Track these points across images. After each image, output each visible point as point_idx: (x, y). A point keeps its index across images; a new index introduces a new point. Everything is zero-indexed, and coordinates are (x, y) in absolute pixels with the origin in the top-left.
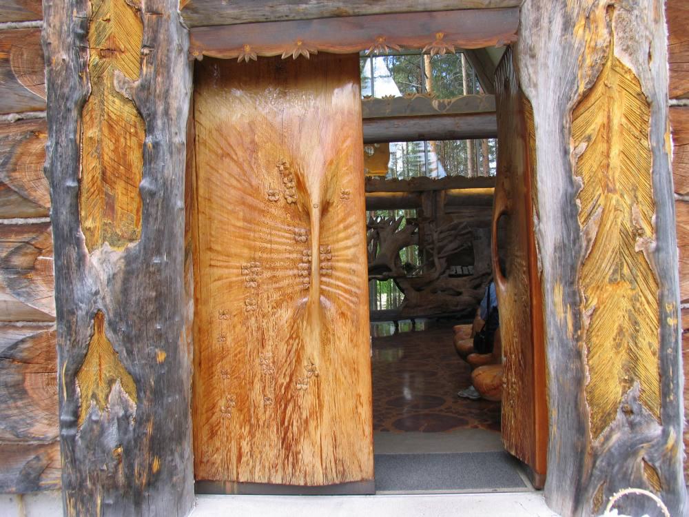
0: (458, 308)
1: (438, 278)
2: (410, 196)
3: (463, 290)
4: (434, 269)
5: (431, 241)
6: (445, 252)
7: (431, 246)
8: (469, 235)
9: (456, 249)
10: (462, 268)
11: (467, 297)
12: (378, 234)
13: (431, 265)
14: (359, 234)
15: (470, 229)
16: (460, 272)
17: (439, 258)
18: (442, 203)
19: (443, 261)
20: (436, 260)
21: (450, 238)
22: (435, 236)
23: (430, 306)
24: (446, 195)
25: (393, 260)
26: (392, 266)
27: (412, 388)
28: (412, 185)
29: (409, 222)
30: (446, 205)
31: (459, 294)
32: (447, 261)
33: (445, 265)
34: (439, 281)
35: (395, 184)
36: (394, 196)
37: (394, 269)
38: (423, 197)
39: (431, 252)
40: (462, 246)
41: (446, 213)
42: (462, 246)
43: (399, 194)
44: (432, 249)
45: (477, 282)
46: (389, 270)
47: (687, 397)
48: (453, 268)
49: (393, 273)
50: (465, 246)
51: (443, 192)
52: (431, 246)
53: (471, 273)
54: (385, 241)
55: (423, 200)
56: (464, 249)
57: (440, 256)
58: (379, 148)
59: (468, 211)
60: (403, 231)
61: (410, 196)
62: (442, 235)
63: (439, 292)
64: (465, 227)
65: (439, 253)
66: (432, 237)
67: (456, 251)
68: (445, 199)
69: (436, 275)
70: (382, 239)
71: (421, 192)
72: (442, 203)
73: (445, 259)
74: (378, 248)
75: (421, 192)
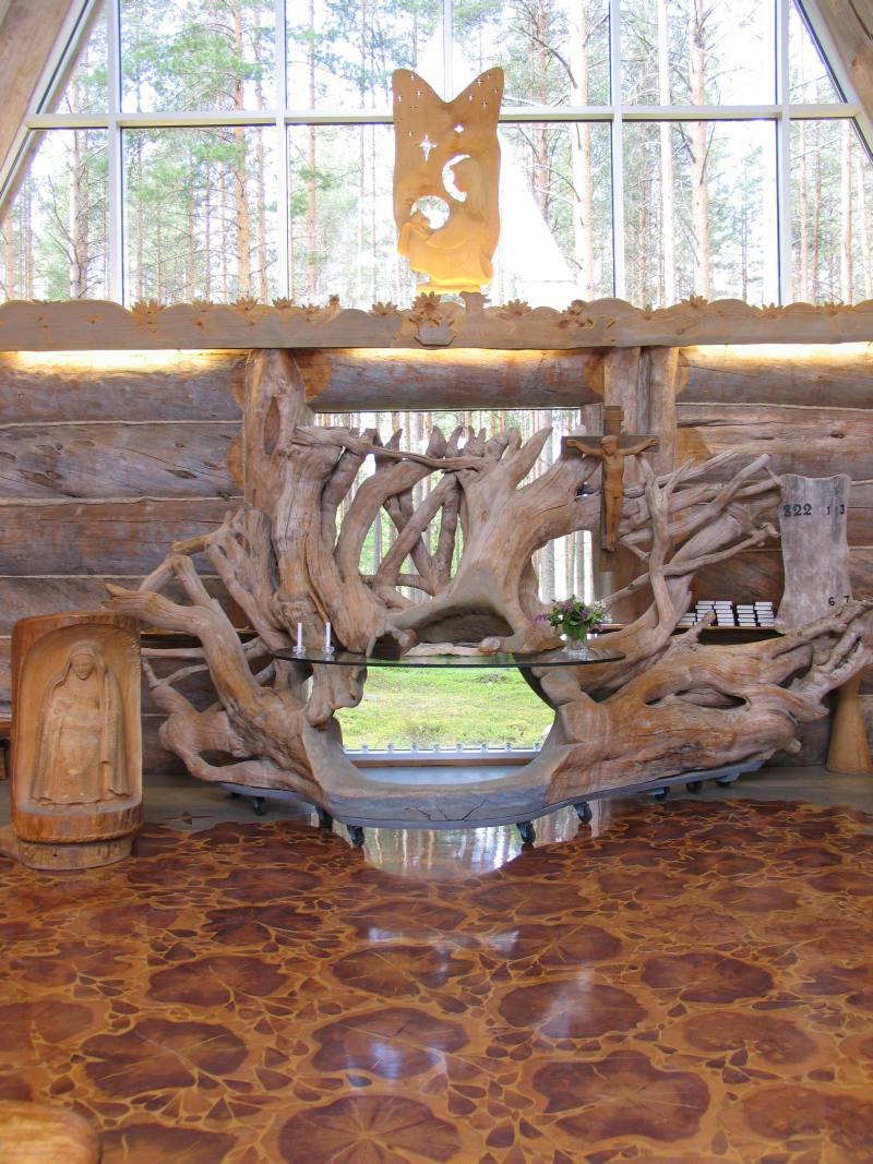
0: (734, 754)
1: (665, 647)
2: (566, 363)
3: (746, 691)
4: (649, 614)
5: (643, 515)
6: (691, 558)
7: (643, 535)
8: (771, 500)
9: (724, 547)
10: (734, 609)
11: (767, 717)
12: (459, 488)
13: (641, 600)
14: (283, 391)
15: (777, 480)
16: (726, 621)
17: (668, 577)
18: (669, 388)
19: (681, 585)
20: (659, 587)
21: (709, 511)
22: (660, 501)
23: (640, 756)
24: (684, 363)
25: (514, 587)
26: (512, 611)
27: (421, 152)
28: (573, 327)
29: (571, 449)
30: (682, 397)
31: (738, 701)
32: (692, 587)
33: (686, 598)
34: (668, 656)
35: (519, 322)
36: (511, 364)
37: (519, 623)
38: (609, 370)
39: (642, 554)
40: (745, 536)
41: (681, 425)
42: (745, 536)
43: (529, 358)
44: (647, 546)
45: (797, 659)
46: (501, 626)
47: (871, 740)
48: (704, 607)
49: (519, 642)
50: (758, 535)
51: (675, 351)
52: (643, 535)
53: (765, 625)
54: (484, 516)
55: (607, 378)
56: (754, 546)
57: (672, 567)
58: (465, 204)
59: (754, 418)
60: (549, 481)
61: (566, 363)
62: (682, 499)
63: (670, 698)
64: (762, 473)
65: (667, 560)
66: (649, 501)
67: (726, 554)
68: (679, 376)
69: (658, 636)
70: (475, 511)
71: (602, 353)
72: (669, 388)
73: (686, 580)
74: (459, 536)
75: (602, 353)
